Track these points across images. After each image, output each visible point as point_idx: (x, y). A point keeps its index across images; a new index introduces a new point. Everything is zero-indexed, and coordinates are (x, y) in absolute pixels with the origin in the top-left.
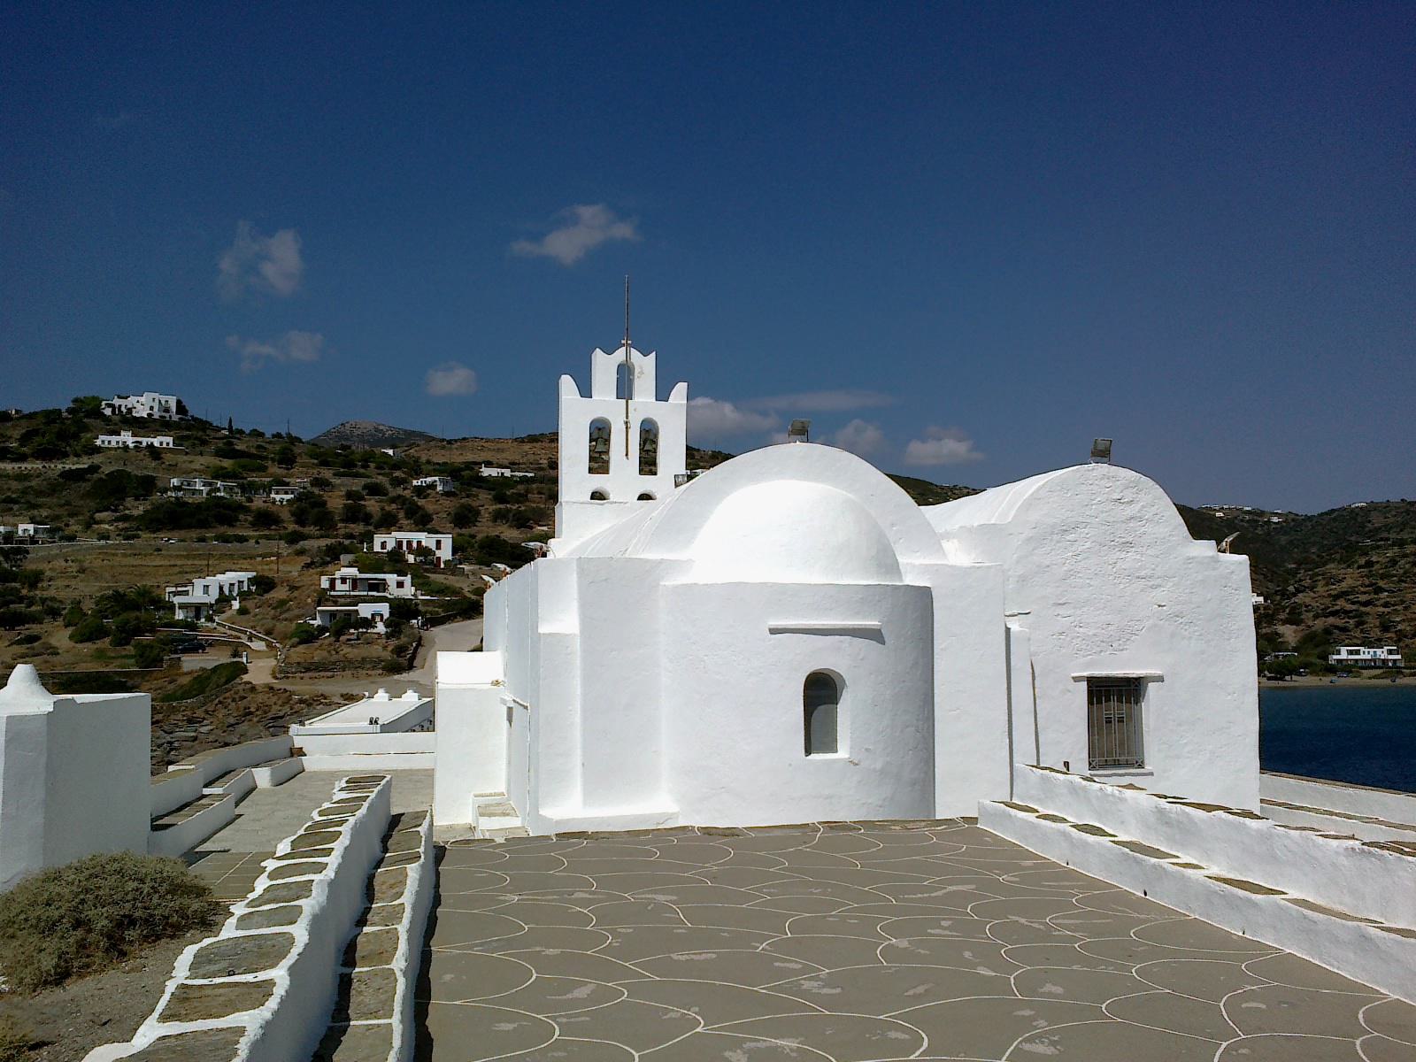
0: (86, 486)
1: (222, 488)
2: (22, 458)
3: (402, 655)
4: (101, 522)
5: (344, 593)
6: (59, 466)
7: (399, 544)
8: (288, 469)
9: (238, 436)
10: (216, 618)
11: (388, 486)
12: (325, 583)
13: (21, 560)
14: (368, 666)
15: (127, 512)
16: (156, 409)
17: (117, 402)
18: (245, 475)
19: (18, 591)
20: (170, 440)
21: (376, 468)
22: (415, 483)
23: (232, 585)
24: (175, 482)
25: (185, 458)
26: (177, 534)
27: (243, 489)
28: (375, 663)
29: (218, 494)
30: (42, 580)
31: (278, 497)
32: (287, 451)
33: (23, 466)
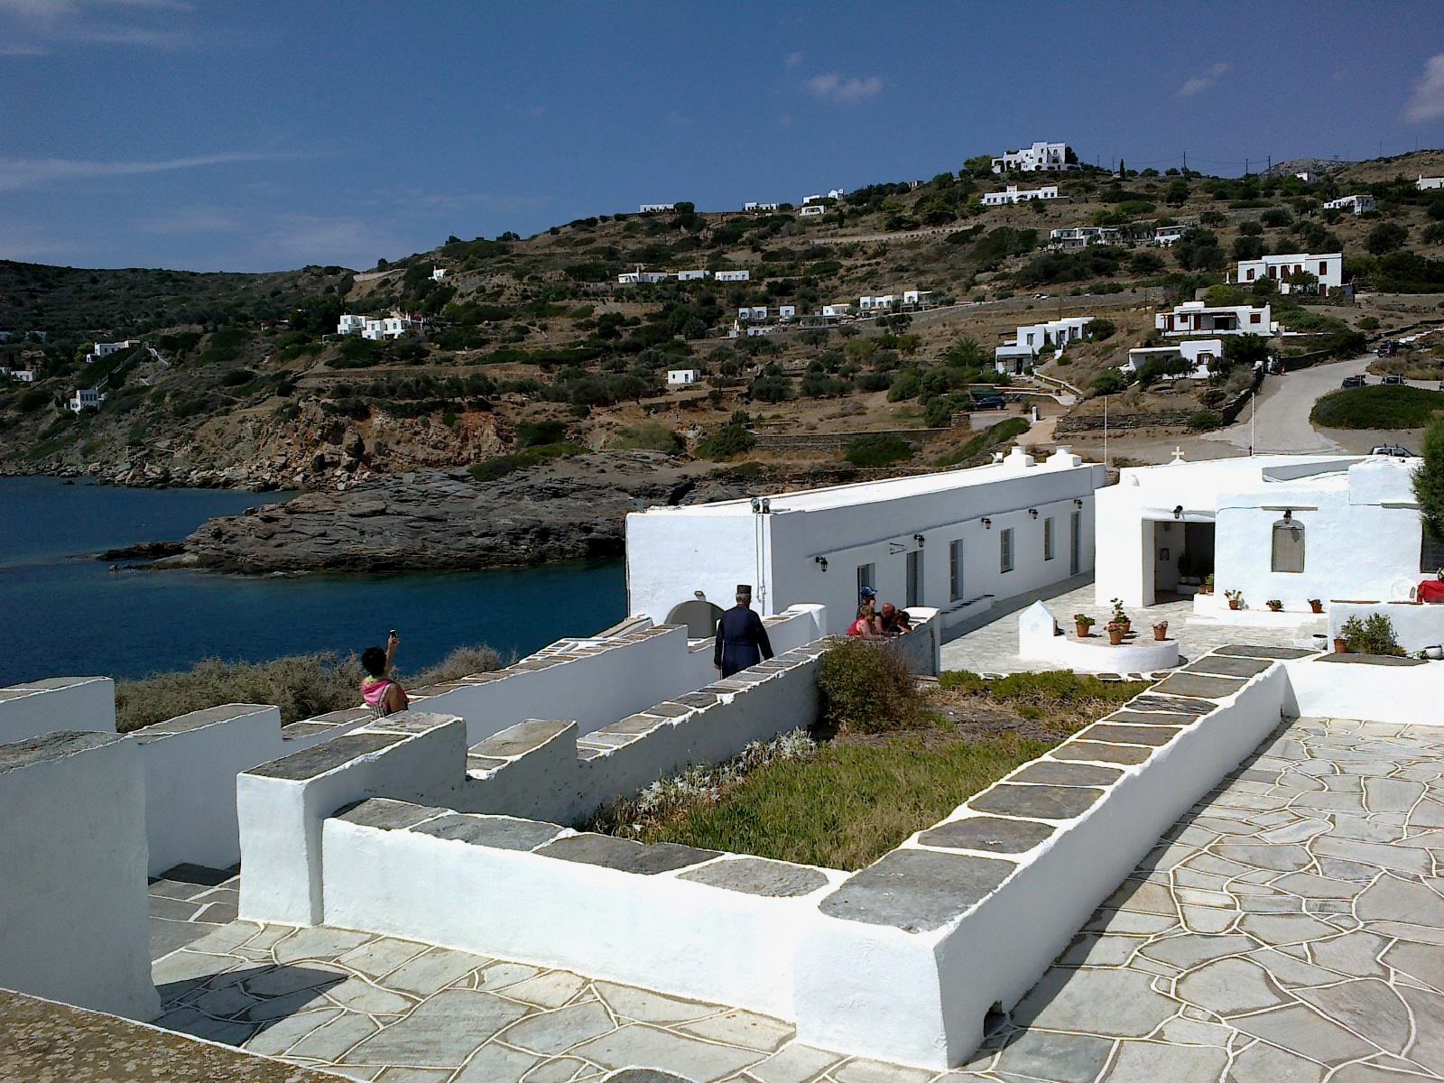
0: (970, 248)
1: (1103, 236)
2: (915, 226)
3: (1216, 404)
4: (980, 283)
5: (1181, 333)
6: (947, 230)
7: (1272, 270)
8: (1178, 207)
9: (1130, 178)
10: (1035, 371)
11: (1292, 212)
12: (1160, 322)
13: (905, 327)
14: (1169, 421)
15: (1007, 270)
16: (1044, 161)
17: (1006, 158)
18: (1130, 219)
19: (896, 355)
20: (1054, 190)
21: (1282, 195)
22: (1326, 206)
23: (1062, 332)
24: (1054, 233)
25: (1069, 207)
26: (1051, 289)
27: (1124, 233)
28: (1179, 417)
29: (1099, 242)
30: (921, 345)
31: (1162, 239)
32: (1179, 188)
33: (915, 233)
